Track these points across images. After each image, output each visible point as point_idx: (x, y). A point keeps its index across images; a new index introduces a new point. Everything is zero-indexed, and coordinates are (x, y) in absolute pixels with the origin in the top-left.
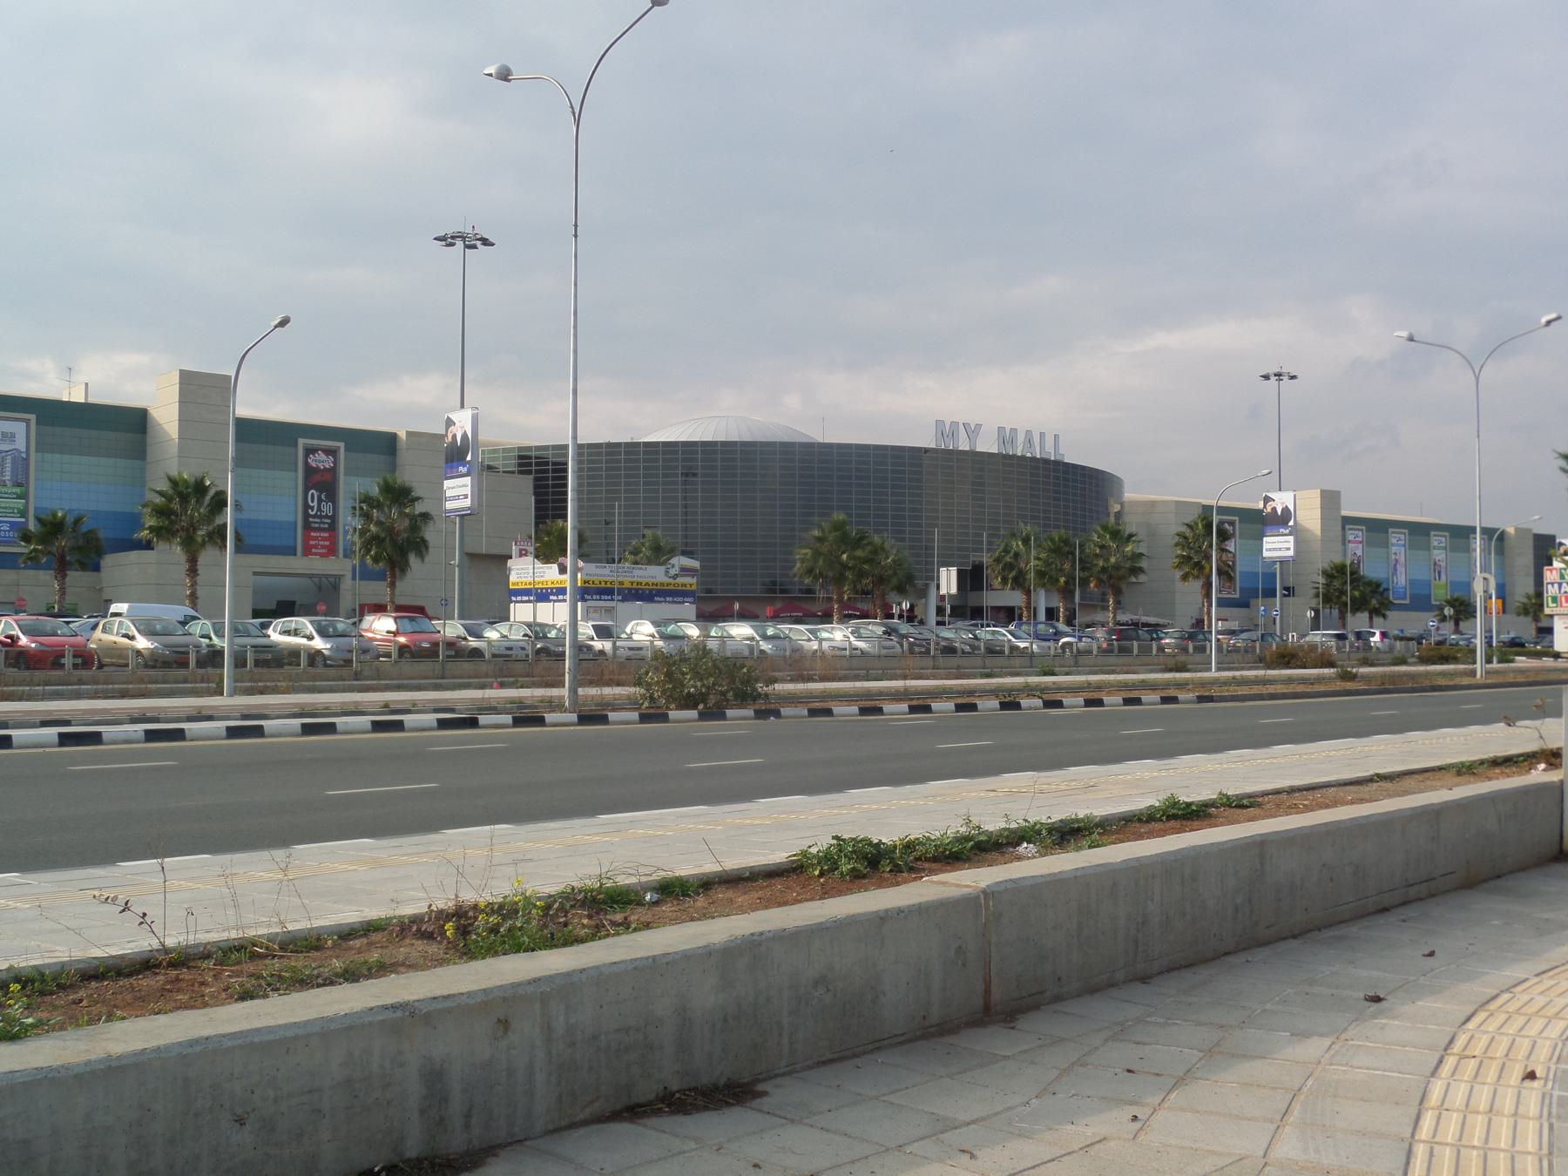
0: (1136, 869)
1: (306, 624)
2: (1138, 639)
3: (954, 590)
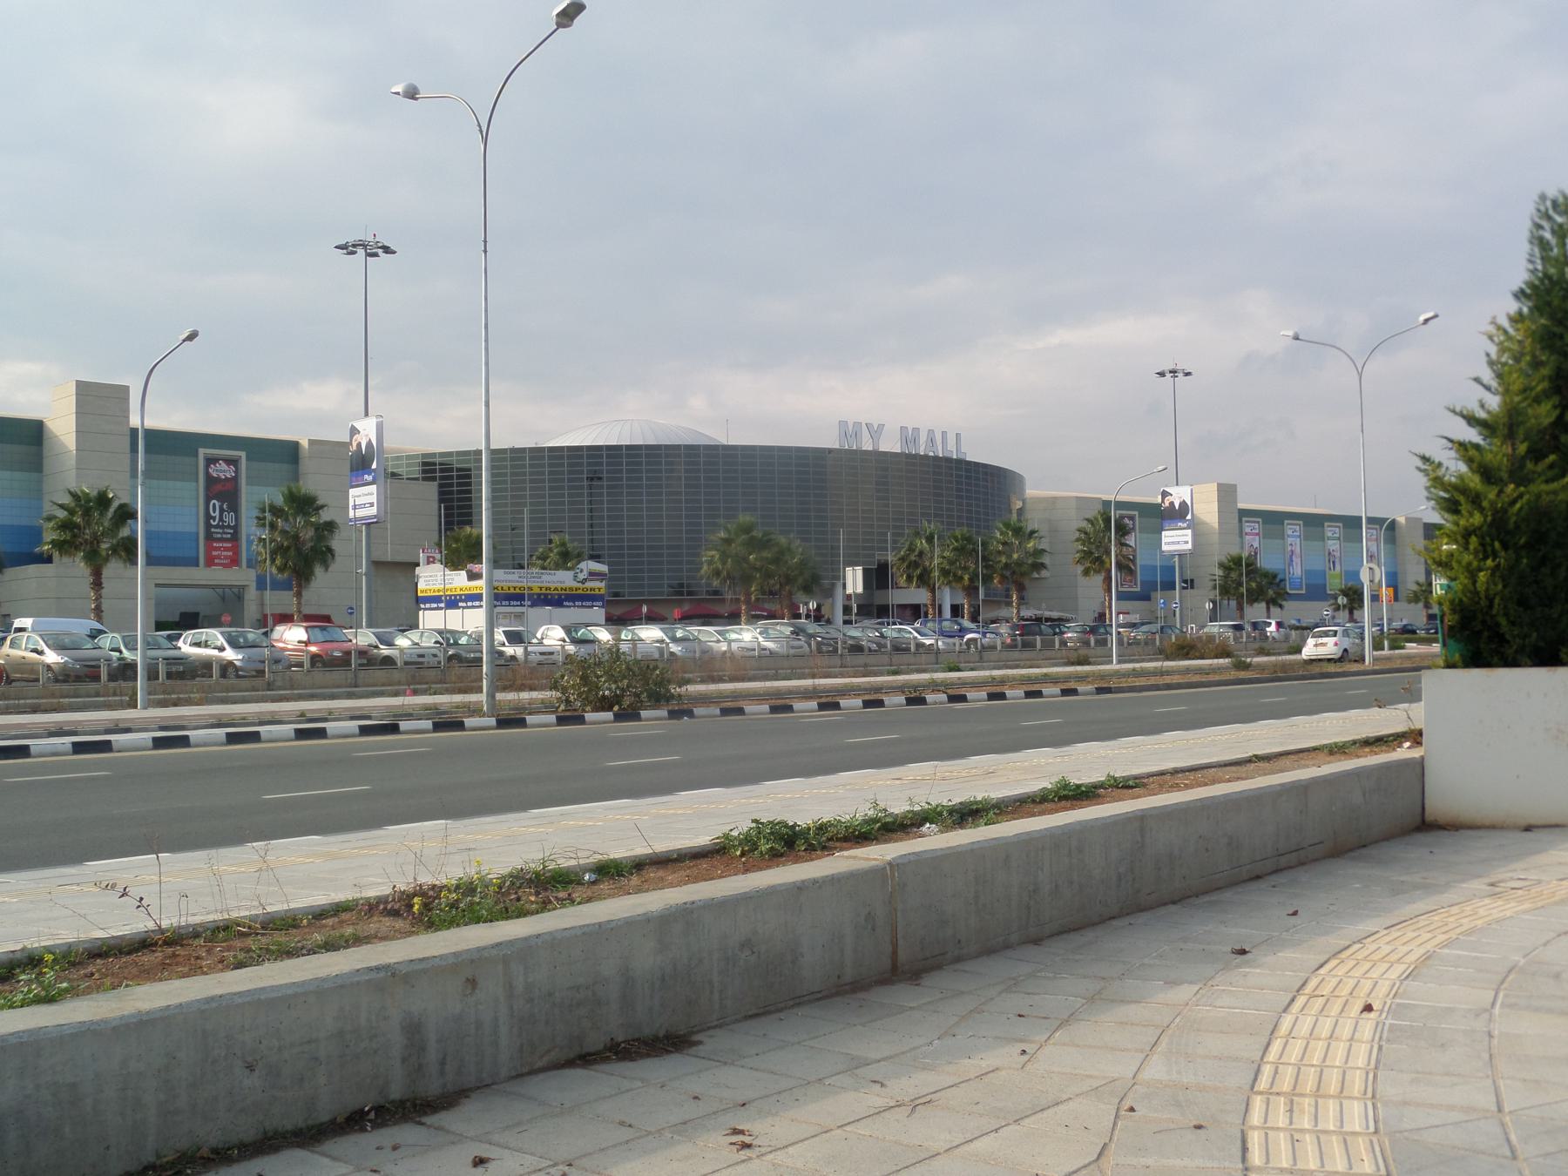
0: (1027, 843)
1: (216, 635)
2: (1041, 633)
3: (860, 590)
